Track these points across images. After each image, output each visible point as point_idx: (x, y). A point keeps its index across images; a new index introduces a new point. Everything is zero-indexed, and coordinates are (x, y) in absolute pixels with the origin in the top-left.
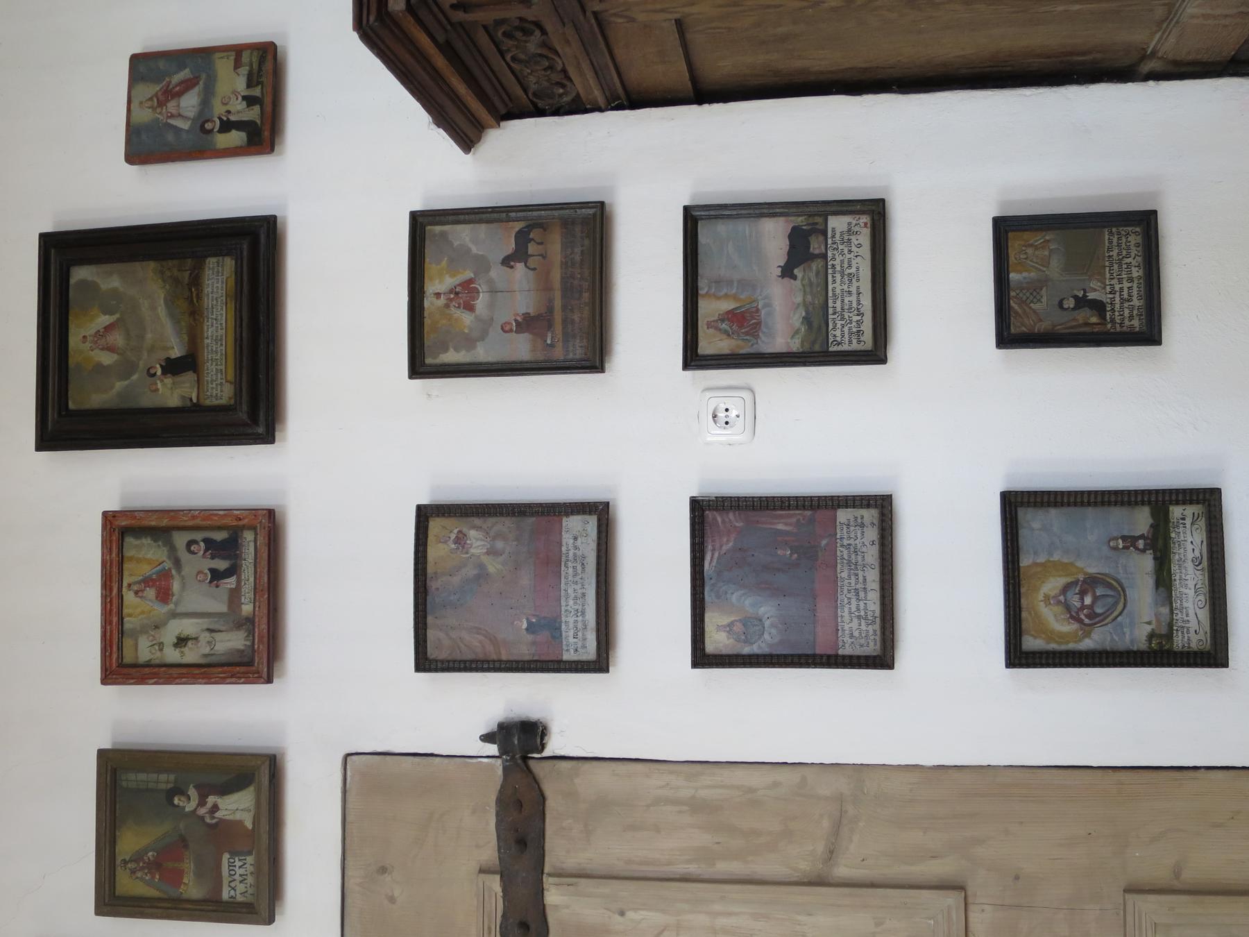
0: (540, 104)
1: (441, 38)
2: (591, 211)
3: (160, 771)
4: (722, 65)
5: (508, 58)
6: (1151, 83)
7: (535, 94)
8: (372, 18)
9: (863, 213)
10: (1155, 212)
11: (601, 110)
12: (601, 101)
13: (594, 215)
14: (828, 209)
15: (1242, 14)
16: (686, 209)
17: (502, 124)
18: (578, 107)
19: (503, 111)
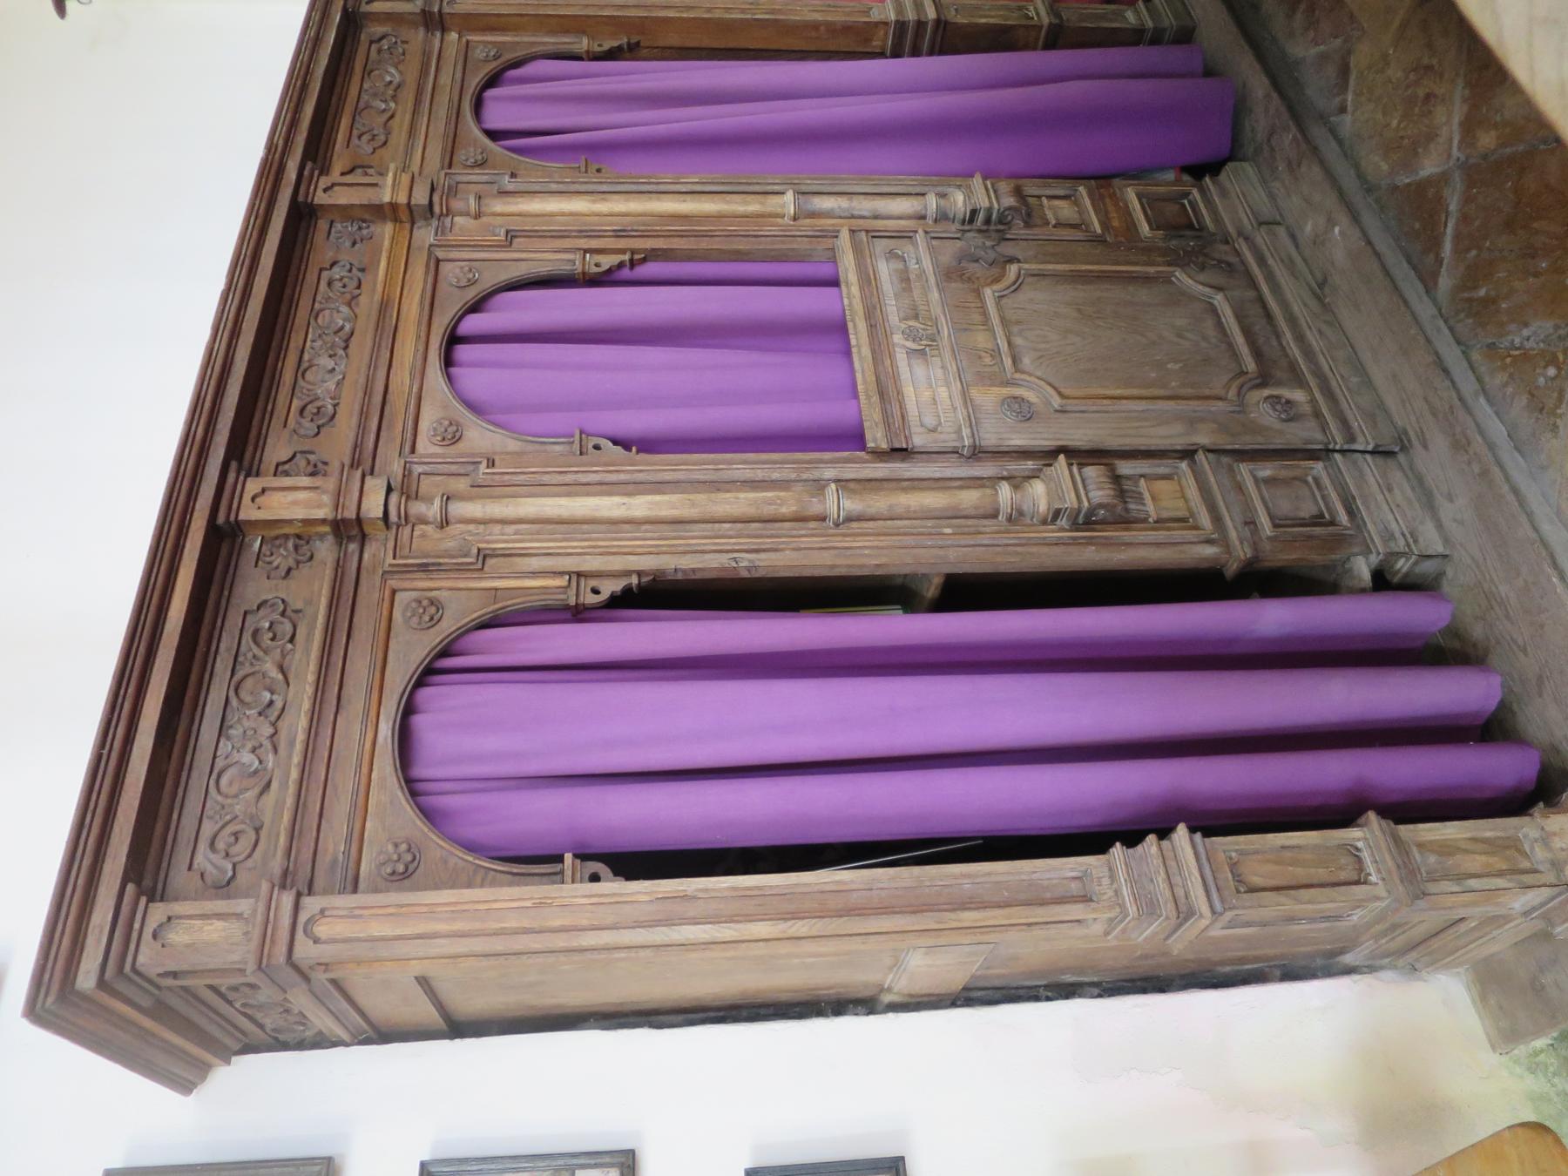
0: (281, 1037)
1: (146, 1002)
2: (317, 1168)
3: (1151, 17)
4: (469, 1004)
5: (238, 1005)
6: (891, 1015)
7: (274, 1030)
8: (50, 1000)
9: (611, 1165)
10: (903, 1158)
11: (347, 1045)
12: (346, 1037)
13: (319, 1173)
14: (575, 1161)
15: (1311, 9)
16: (423, 1165)
17: (234, 1059)
18: (321, 1042)
19: (237, 1047)
